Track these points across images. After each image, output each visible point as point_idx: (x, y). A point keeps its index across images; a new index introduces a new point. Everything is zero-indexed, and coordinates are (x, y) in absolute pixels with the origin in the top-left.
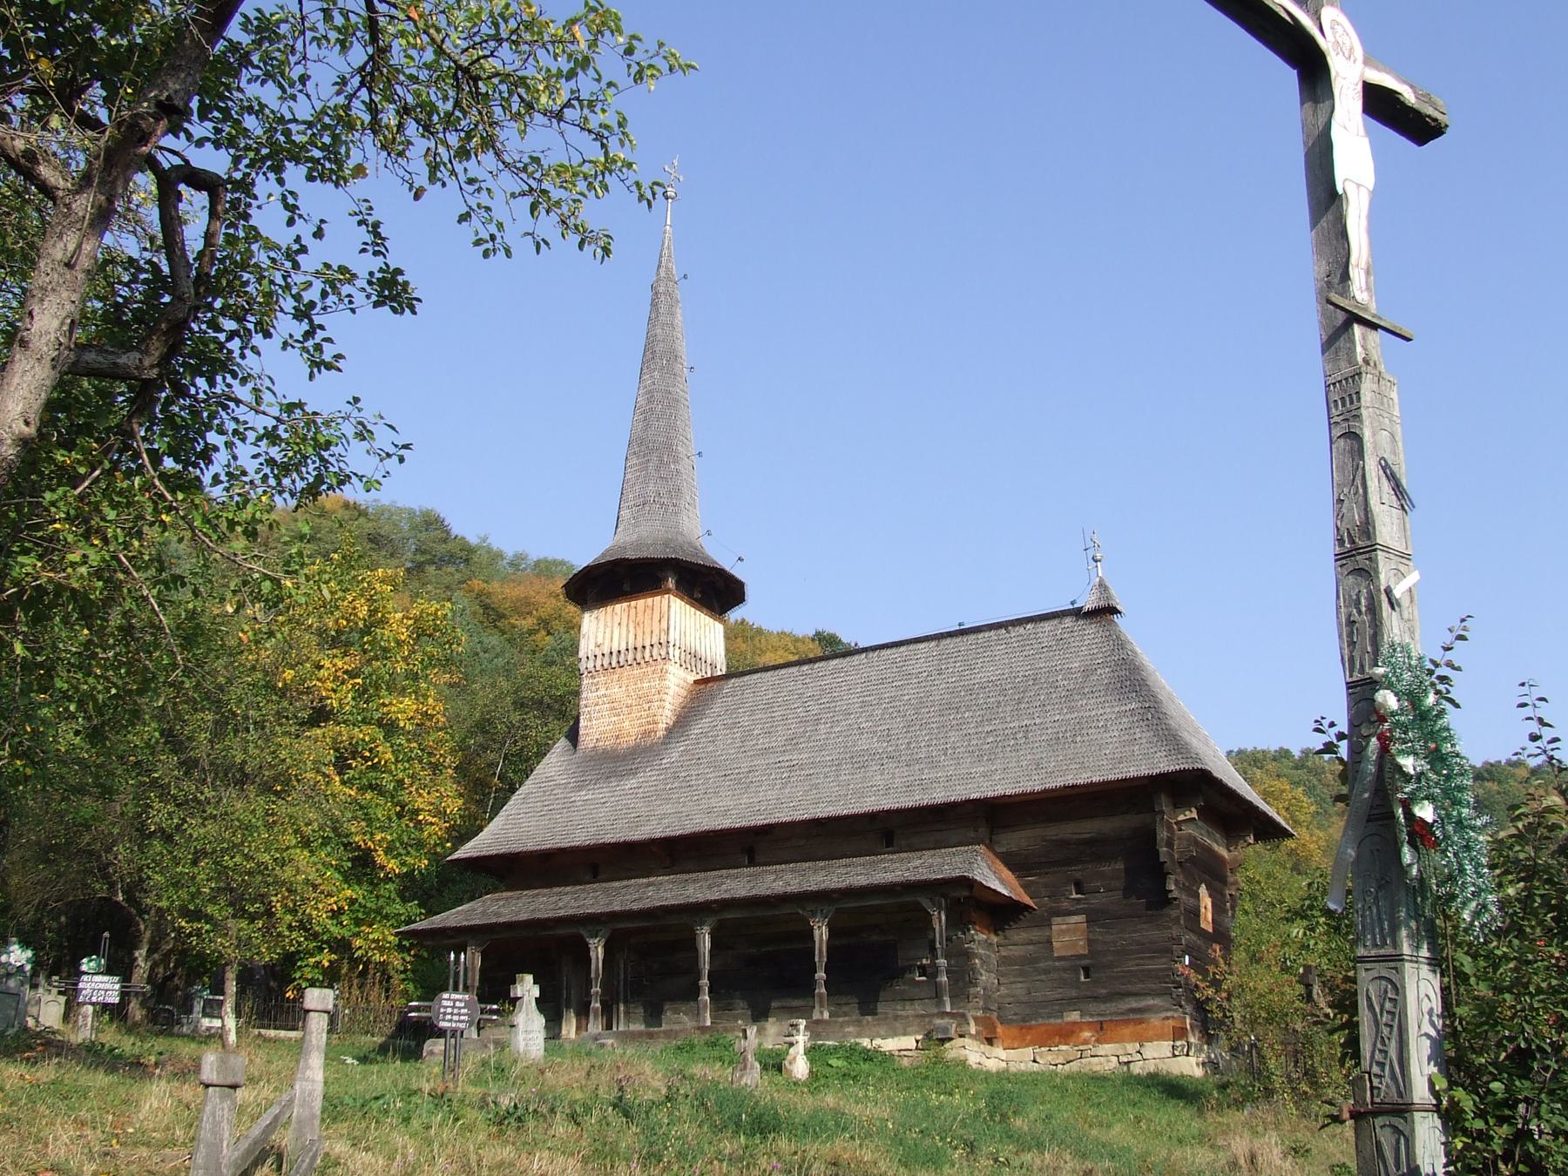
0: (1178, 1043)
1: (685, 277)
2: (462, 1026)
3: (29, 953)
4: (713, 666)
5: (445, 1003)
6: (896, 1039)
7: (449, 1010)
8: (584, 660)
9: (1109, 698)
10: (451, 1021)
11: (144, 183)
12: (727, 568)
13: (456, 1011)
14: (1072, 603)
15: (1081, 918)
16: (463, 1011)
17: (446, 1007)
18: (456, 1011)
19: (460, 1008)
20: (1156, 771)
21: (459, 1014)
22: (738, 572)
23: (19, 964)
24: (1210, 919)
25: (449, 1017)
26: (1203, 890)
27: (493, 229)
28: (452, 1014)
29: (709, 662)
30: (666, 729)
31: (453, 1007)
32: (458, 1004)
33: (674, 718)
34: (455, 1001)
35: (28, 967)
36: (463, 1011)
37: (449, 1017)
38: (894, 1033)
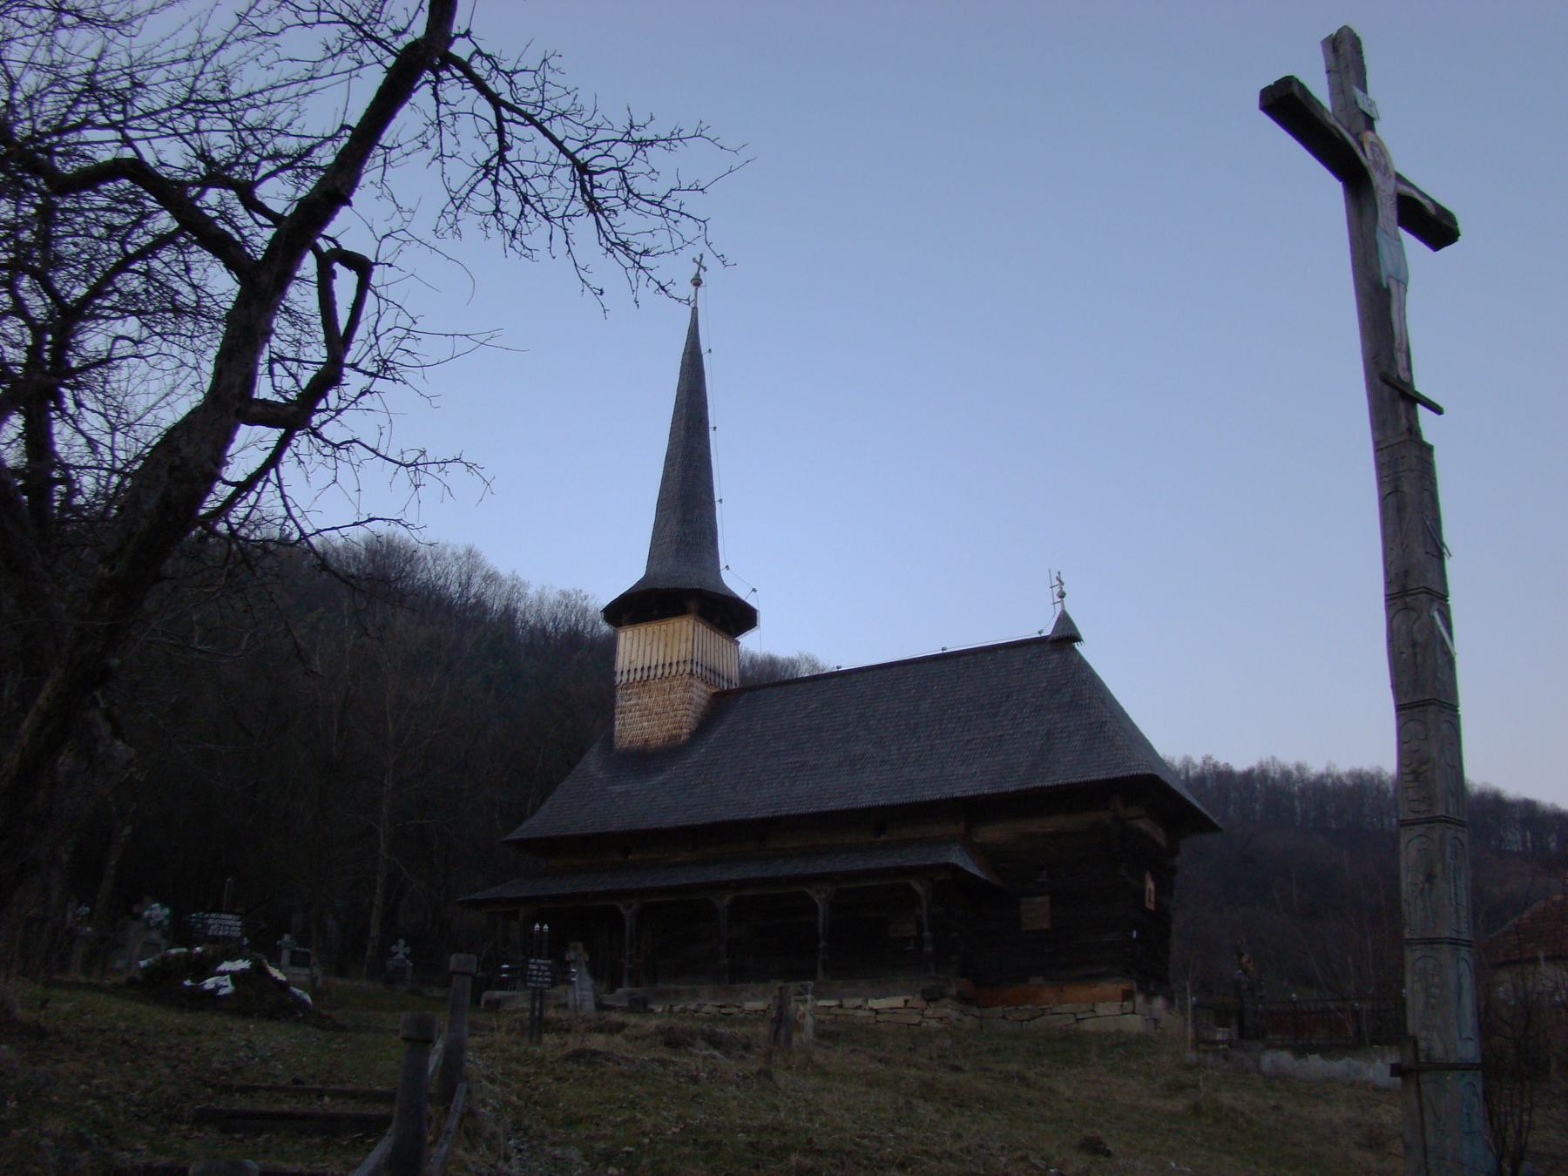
0: (1125, 1003)
1: (710, 351)
2: (545, 986)
3: (167, 911)
4: (729, 681)
5: (532, 967)
6: (888, 999)
7: (535, 973)
8: (619, 674)
9: (1071, 713)
10: (536, 982)
11: (309, 265)
12: (743, 598)
13: (540, 974)
14: (1040, 632)
15: (1046, 899)
16: (547, 973)
17: (533, 970)
18: (540, 974)
19: (544, 971)
20: (1112, 776)
21: (543, 977)
22: (751, 601)
23: (159, 919)
24: (1153, 899)
25: (534, 978)
26: (1148, 876)
27: (407, 323)
28: (537, 976)
29: (725, 677)
30: (690, 734)
31: (539, 970)
32: (542, 968)
33: (696, 725)
34: (540, 965)
35: (166, 922)
36: (547, 973)
37: (534, 978)
38: (886, 995)
